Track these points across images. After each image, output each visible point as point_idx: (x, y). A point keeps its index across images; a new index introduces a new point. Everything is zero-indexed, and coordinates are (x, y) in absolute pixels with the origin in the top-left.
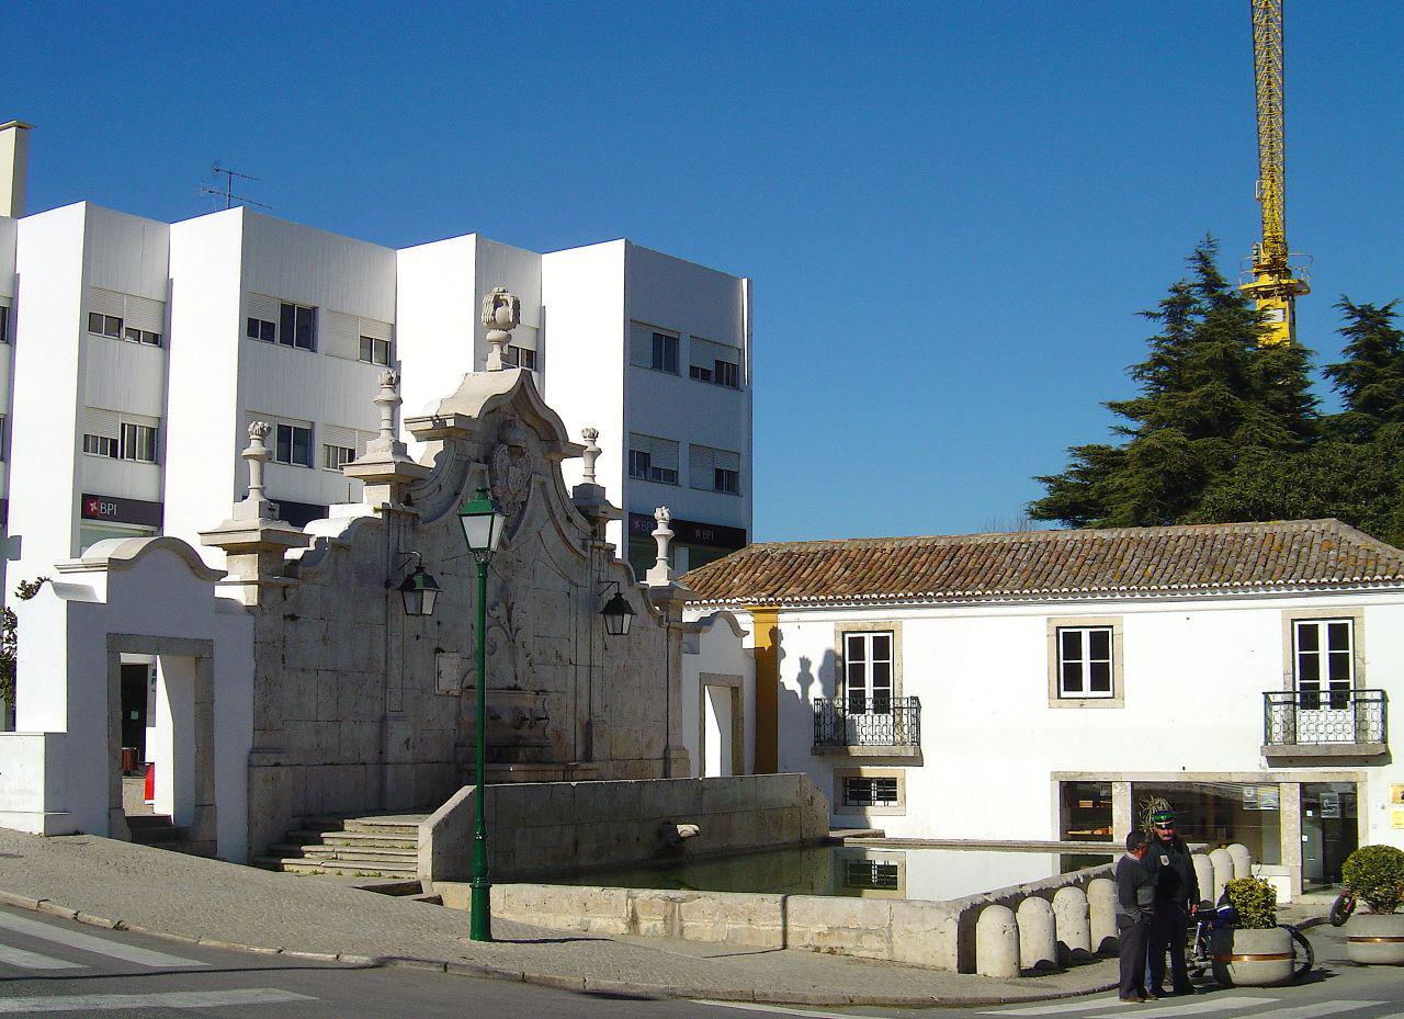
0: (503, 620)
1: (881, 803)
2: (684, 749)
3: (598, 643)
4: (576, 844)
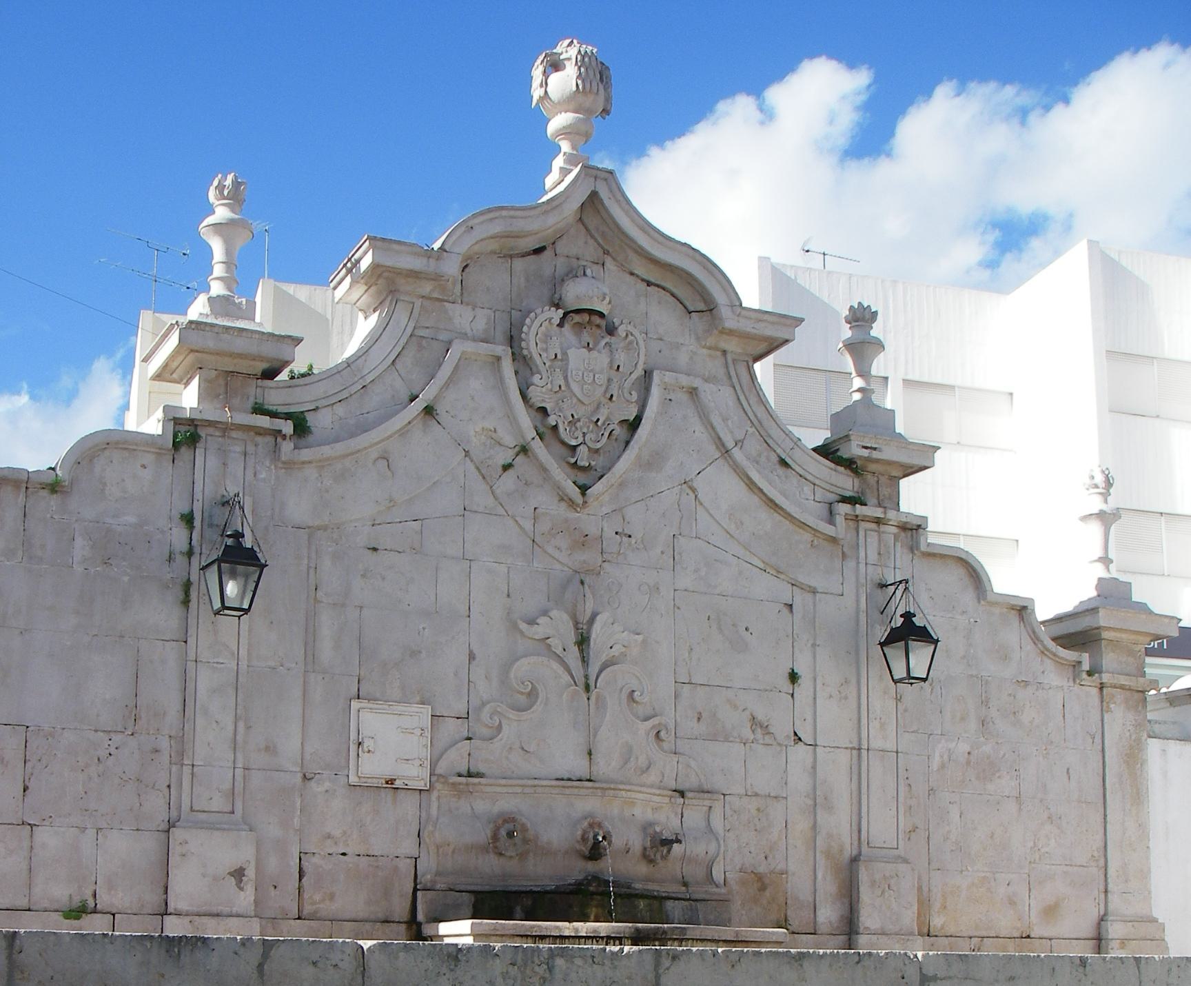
2: (1155, 920)
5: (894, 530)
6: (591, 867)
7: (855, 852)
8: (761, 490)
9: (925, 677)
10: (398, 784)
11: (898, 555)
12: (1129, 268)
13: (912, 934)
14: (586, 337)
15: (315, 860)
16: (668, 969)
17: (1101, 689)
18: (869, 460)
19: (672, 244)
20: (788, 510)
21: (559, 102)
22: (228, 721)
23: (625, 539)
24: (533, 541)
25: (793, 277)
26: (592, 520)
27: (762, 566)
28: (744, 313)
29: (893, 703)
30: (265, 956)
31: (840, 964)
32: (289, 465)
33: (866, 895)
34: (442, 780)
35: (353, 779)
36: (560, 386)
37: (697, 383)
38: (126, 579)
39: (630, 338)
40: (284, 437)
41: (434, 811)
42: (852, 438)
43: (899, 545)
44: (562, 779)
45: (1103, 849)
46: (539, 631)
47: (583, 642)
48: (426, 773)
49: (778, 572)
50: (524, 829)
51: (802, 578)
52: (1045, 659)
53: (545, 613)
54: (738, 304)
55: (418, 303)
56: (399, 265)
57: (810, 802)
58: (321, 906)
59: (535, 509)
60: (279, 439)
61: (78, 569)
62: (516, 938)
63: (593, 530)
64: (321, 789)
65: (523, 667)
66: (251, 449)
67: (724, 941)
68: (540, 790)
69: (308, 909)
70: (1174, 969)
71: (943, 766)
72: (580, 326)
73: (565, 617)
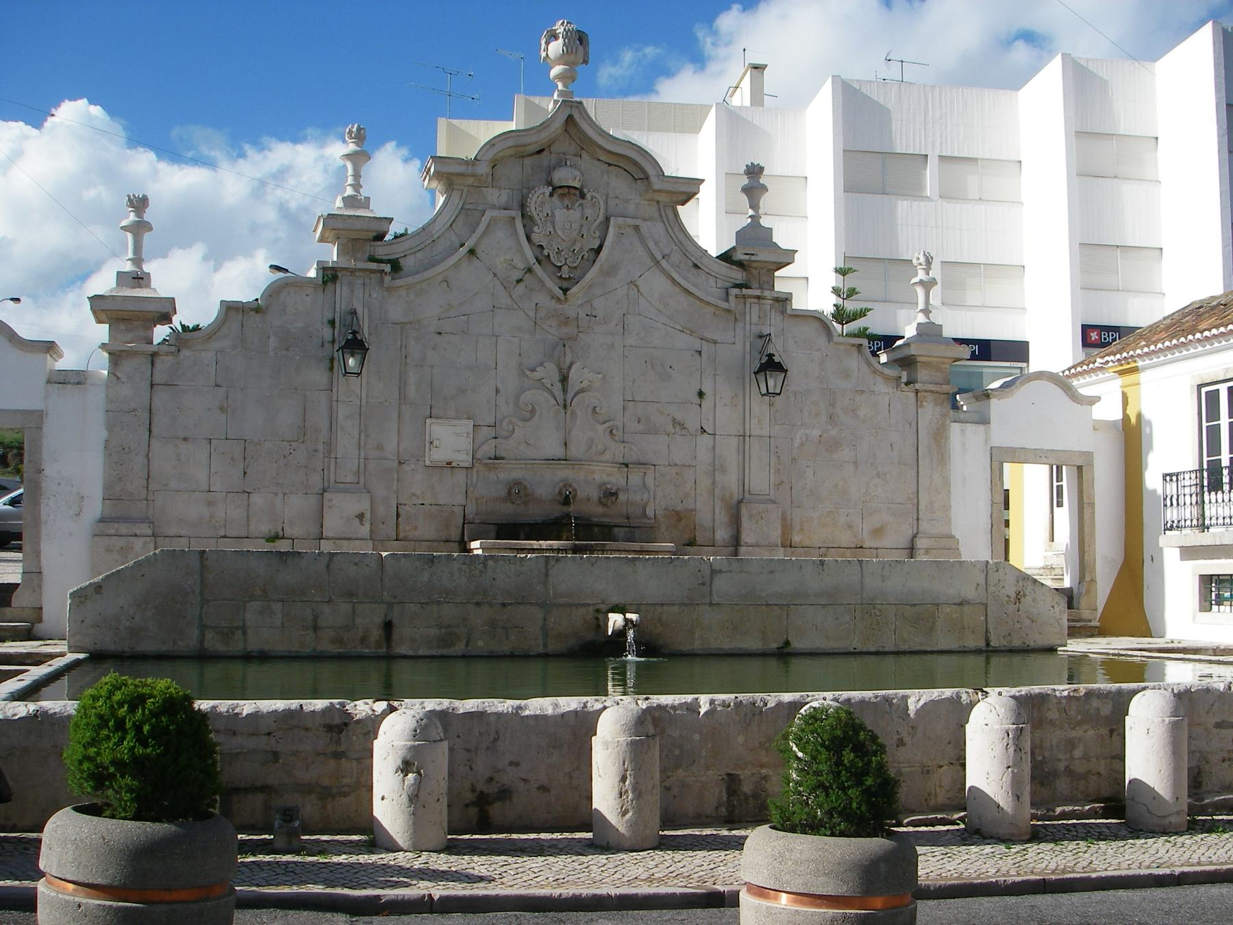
2: (953, 537)
4: (388, 626)
6: (565, 509)
7: (741, 497)
9: (779, 392)
10: (454, 464)
11: (772, 317)
12: (1095, 71)
13: (777, 546)
14: (566, 202)
15: (407, 508)
16: (553, 566)
17: (917, 393)
20: (697, 294)
21: (555, 60)
22: (356, 433)
24: (535, 323)
25: (858, 88)
26: (569, 309)
28: (665, 179)
30: (331, 560)
31: (659, 564)
33: (745, 523)
34: (479, 462)
35: (428, 463)
36: (550, 232)
37: (638, 222)
38: (298, 358)
39: (594, 199)
40: (386, 273)
41: (475, 480)
42: (737, 249)
43: (773, 311)
44: (549, 460)
45: (916, 493)
46: (537, 375)
47: (564, 380)
49: (693, 332)
50: (525, 488)
51: (708, 335)
52: (876, 375)
53: (542, 364)
54: (661, 174)
56: (451, 171)
57: (711, 468)
58: (410, 533)
59: (536, 304)
60: (383, 275)
61: (272, 353)
62: (508, 551)
63: (572, 314)
65: (527, 396)
66: (367, 281)
67: (634, 551)
68: (535, 466)
69: (402, 535)
70: (887, 566)
71: (802, 444)
72: (563, 196)
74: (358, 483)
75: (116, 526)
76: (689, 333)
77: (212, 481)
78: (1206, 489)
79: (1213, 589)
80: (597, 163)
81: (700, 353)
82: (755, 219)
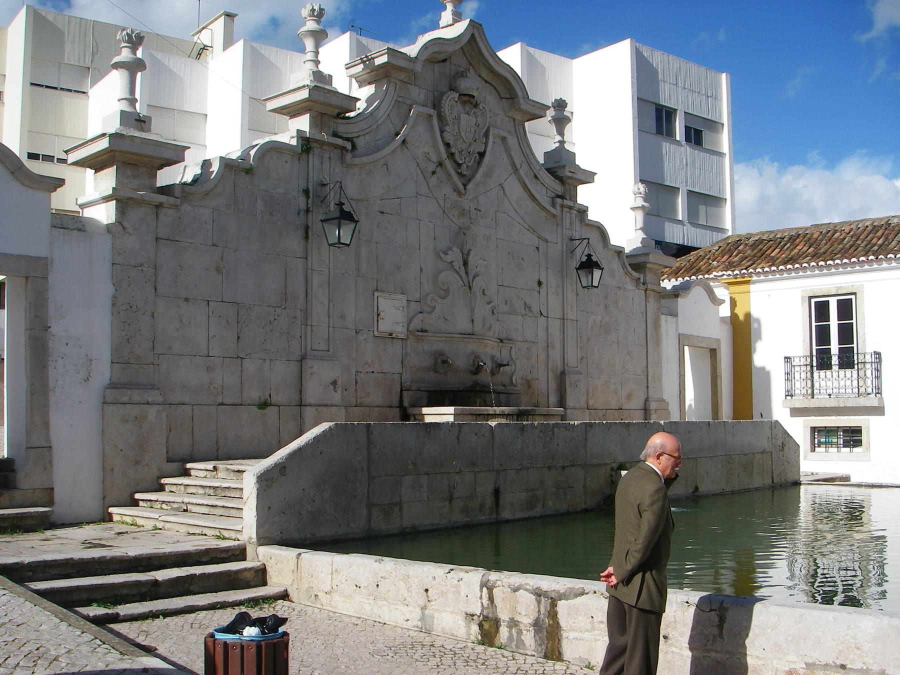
0: (459, 263)
1: (848, 449)
2: (664, 401)
3: (571, 297)
4: (497, 493)
5: (575, 212)
8: (529, 190)
10: (394, 336)
18: (569, 177)
19: (502, 64)
23: (479, 212)
27: (528, 227)
29: (575, 296)
32: (349, 166)
35: (376, 333)
37: (506, 135)
38: (280, 223)
40: (347, 151)
47: (465, 264)
48: (404, 330)
49: (534, 231)
55: (398, 83)
58: (365, 399)
60: (344, 152)
64: (363, 338)
65: (442, 277)
71: (592, 328)
73: (459, 251)
74: (329, 351)
75: (129, 393)
76: (532, 231)
77: (211, 345)
78: (815, 368)
79: (816, 436)
80: (479, 79)
81: (538, 248)
82: (562, 143)
